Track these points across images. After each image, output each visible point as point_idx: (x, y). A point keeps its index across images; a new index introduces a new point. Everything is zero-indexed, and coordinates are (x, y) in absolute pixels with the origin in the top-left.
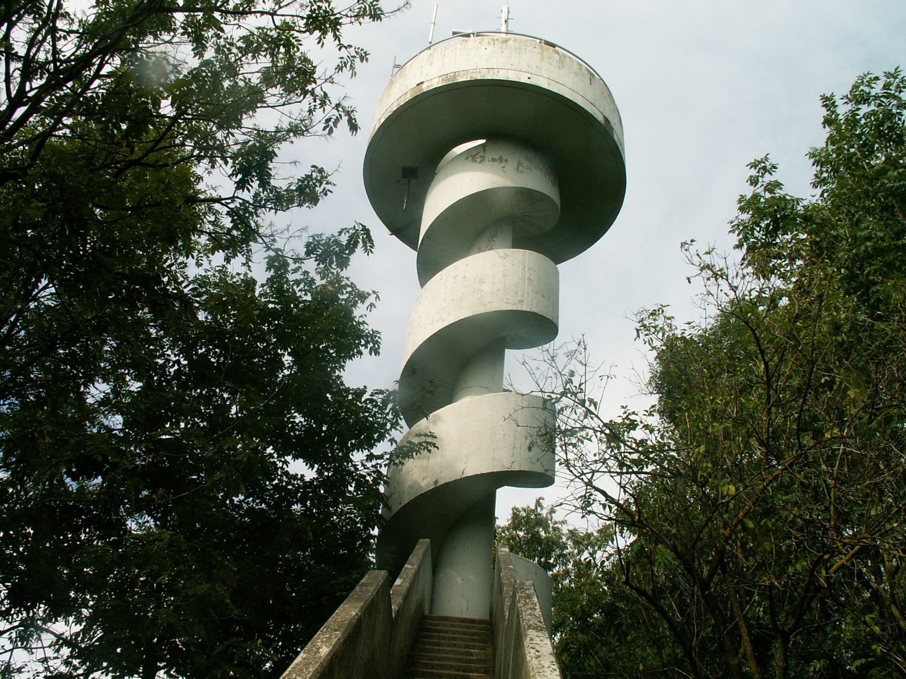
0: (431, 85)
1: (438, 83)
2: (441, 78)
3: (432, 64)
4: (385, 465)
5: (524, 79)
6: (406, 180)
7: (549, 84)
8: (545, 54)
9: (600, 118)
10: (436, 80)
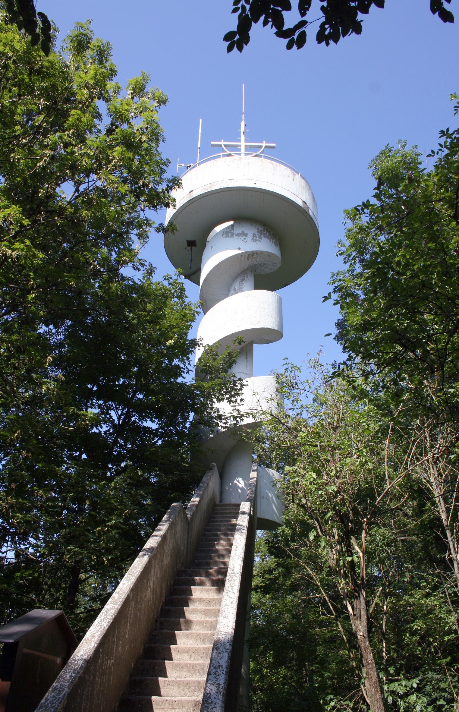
9: (300, 203)
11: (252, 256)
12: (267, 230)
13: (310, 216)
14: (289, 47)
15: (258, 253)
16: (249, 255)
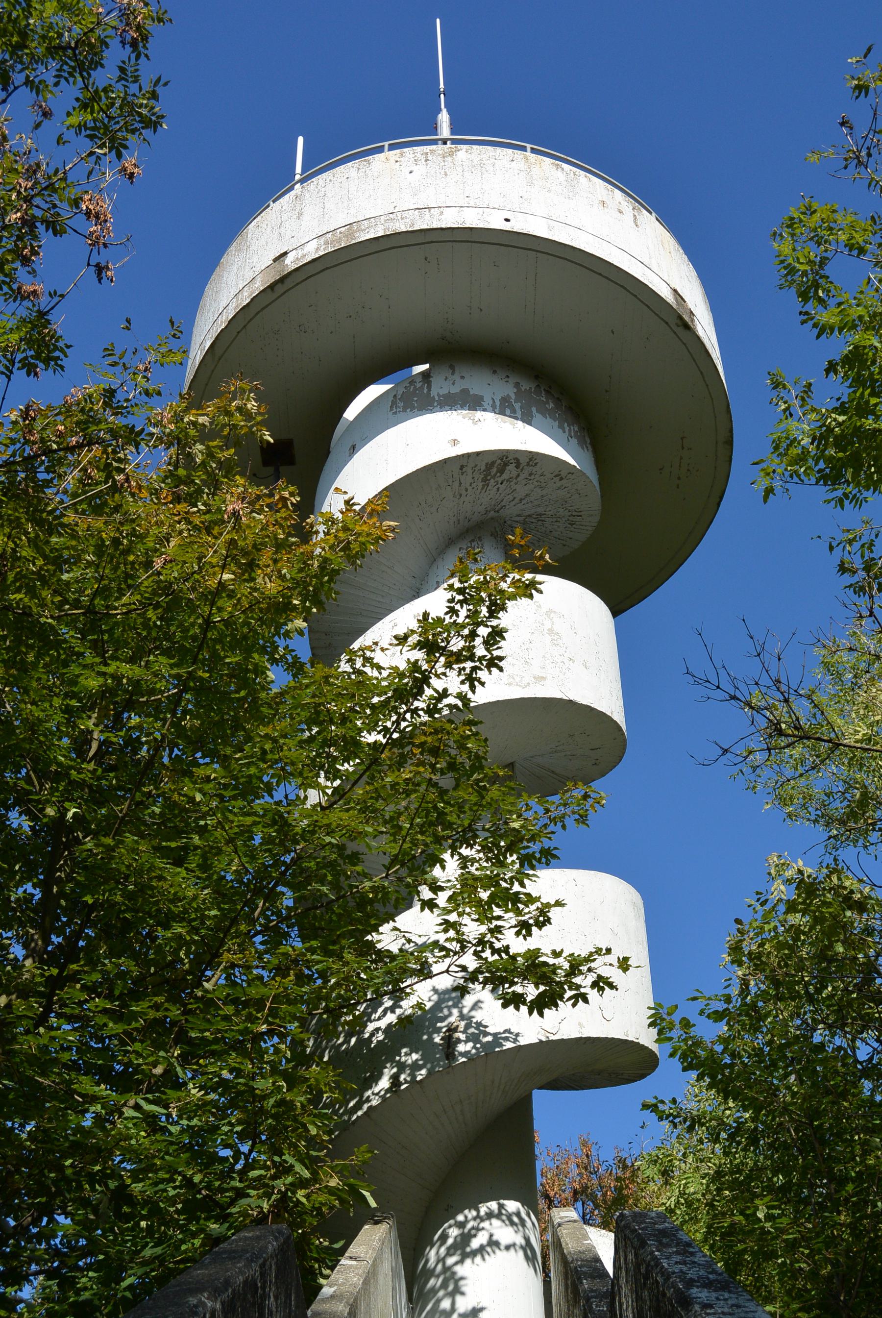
0: (304, 256)
1: (317, 249)
2: (322, 240)
3: (300, 215)
4: (519, 913)
5: (496, 223)
6: (270, 470)
7: (550, 229)
8: (536, 170)
9: (666, 294)
10: (313, 245)
11: (501, 471)
12: (547, 392)
13: (698, 338)
14: (525, 939)
15: (523, 461)
16: (489, 466)
